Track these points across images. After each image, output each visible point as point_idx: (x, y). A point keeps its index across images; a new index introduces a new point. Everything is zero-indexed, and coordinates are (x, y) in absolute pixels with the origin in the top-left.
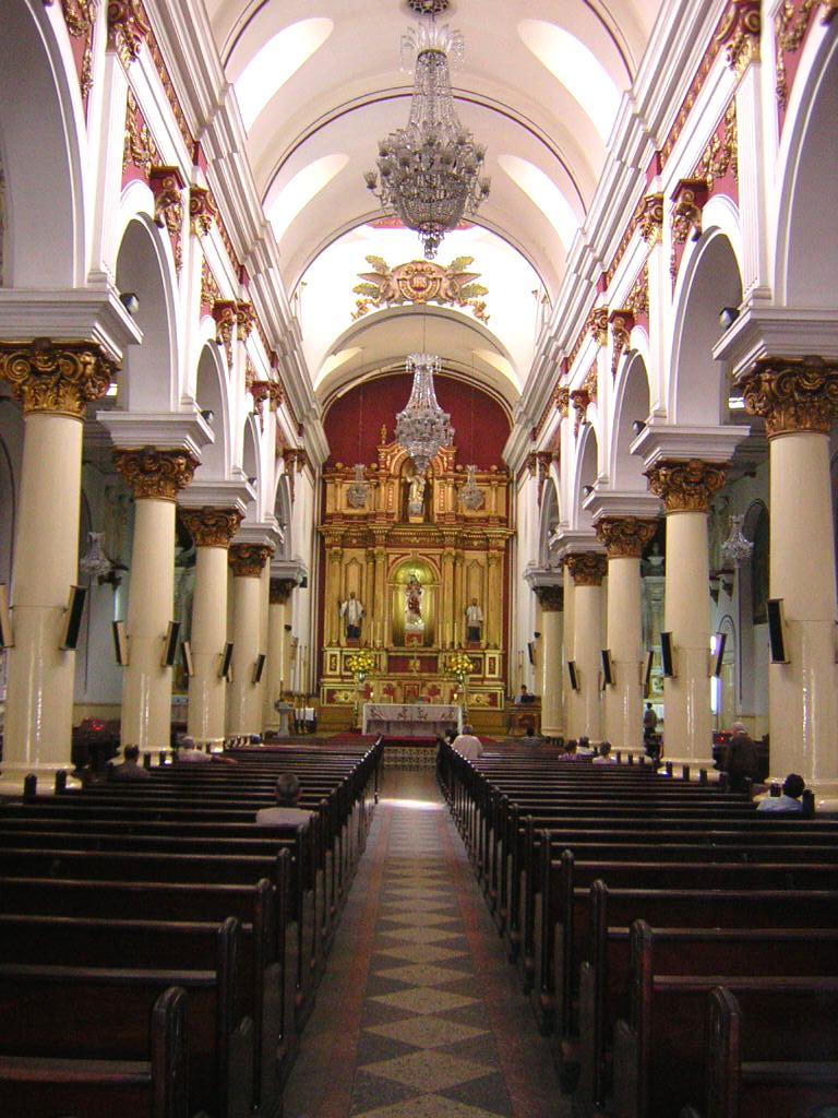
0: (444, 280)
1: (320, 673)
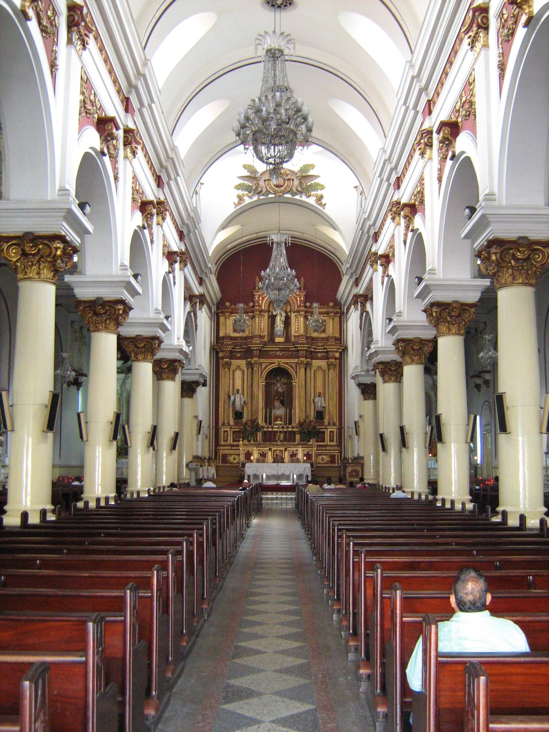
0: (295, 180)
1: (217, 444)
